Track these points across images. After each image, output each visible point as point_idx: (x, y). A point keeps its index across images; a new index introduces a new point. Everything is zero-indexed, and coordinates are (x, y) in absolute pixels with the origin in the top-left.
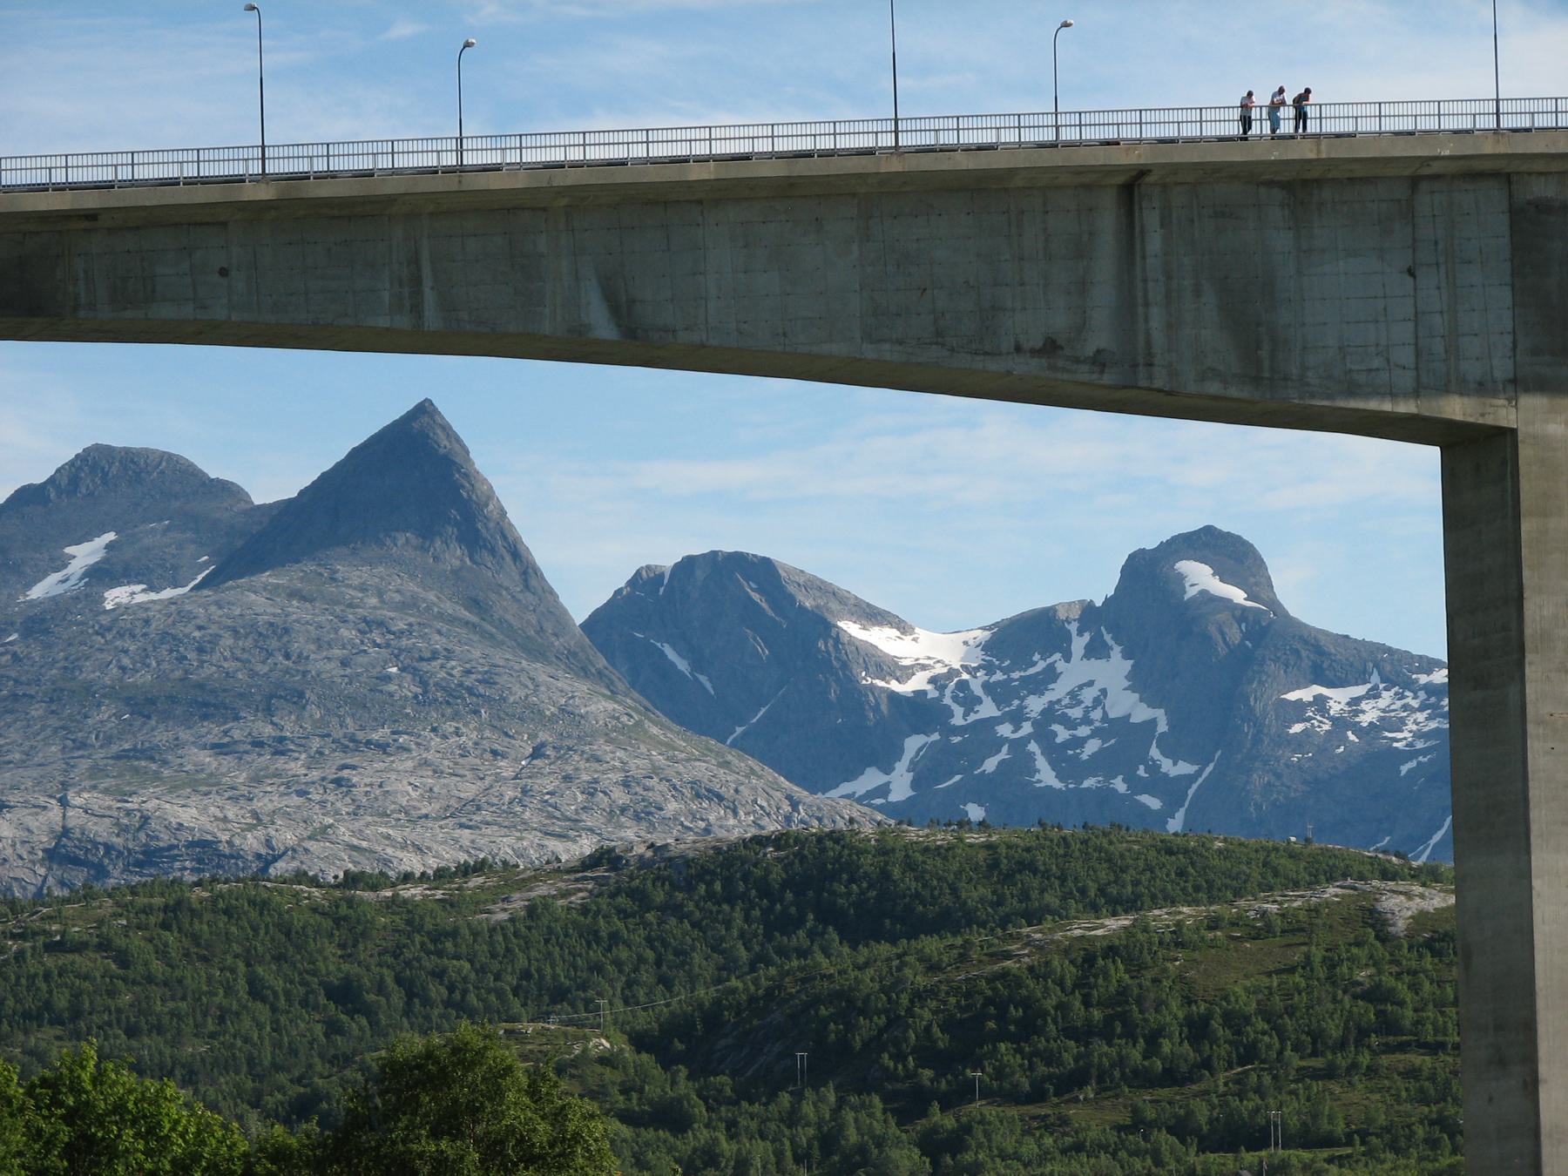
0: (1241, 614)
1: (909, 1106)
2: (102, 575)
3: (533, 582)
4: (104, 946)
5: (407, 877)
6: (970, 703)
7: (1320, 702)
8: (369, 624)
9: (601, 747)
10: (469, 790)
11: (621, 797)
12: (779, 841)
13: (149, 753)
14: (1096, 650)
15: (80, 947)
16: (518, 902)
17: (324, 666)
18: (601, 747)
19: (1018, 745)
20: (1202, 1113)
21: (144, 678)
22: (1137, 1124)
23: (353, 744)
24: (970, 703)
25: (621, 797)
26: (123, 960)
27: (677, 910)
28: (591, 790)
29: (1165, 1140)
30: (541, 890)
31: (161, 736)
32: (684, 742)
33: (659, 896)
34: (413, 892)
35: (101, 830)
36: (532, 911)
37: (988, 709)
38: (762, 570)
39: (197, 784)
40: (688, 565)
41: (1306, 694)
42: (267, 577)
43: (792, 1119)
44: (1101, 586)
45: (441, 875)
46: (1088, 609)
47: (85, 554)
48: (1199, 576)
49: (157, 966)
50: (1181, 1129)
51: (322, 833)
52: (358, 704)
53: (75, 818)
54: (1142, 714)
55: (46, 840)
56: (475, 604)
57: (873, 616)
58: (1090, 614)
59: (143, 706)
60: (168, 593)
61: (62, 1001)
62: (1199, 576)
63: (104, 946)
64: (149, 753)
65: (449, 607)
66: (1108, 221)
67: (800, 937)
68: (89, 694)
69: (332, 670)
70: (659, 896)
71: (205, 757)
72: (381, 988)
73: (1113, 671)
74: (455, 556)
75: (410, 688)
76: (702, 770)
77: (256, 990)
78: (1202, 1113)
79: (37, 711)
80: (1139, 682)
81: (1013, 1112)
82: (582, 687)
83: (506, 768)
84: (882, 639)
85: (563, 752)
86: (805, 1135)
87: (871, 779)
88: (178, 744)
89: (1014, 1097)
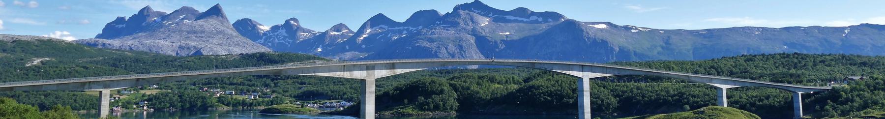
4: (193, 62)
5: (222, 55)
6: (270, 33)
9: (234, 38)
10: (221, 42)
11: (236, 43)
12: (258, 53)
13: (189, 37)
15: (190, 62)
16: (233, 58)
17: (207, 29)
18: (234, 38)
20: (299, 81)
21: (188, 30)
22: (294, 82)
23: (209, 37)
24: (270, 33)
25: (236, 43)
27: (248, 59)
28: (233, 42)
29: (296, 84)
30: (235, 57)
32: (242, 37)
33: (247, 58)
35: (184, 45)
37: (271, 34)
38: (250, 20)
39: (194, 40)
40: (242, 20)
41: (302, 34)
43: (262, 81)
44: (283, 23)
45: (225, 55)
46: (282, 25)
47: (182, 17)
48: (292, 22)
49: (198, 64)
50: (298, 83)
51: (206, 46)
52: (210, 33)
53: (181, 44)
56: (222, 23)
57: (261, 25)
59: (188, 32)
60: (191, 21)
61: (189, 67)
62: (292, 22)
64: (189, 37)
65: (290, 66)
67: (260, 62)
68: (183, 31)
69: (208, 30)
70: (247, 58)
71: (194, 38)
72: (220, 66)
74: (220, 18)
75: (215, 31)
76: (244, 40)
77: (208, 66)
78: (299, 81)
80: (286, 32)
81: (282, 81)
82: (232, 32)
83: (225, 40)
84: (261, 27)
86: (263, 82)
88: (191, 36)
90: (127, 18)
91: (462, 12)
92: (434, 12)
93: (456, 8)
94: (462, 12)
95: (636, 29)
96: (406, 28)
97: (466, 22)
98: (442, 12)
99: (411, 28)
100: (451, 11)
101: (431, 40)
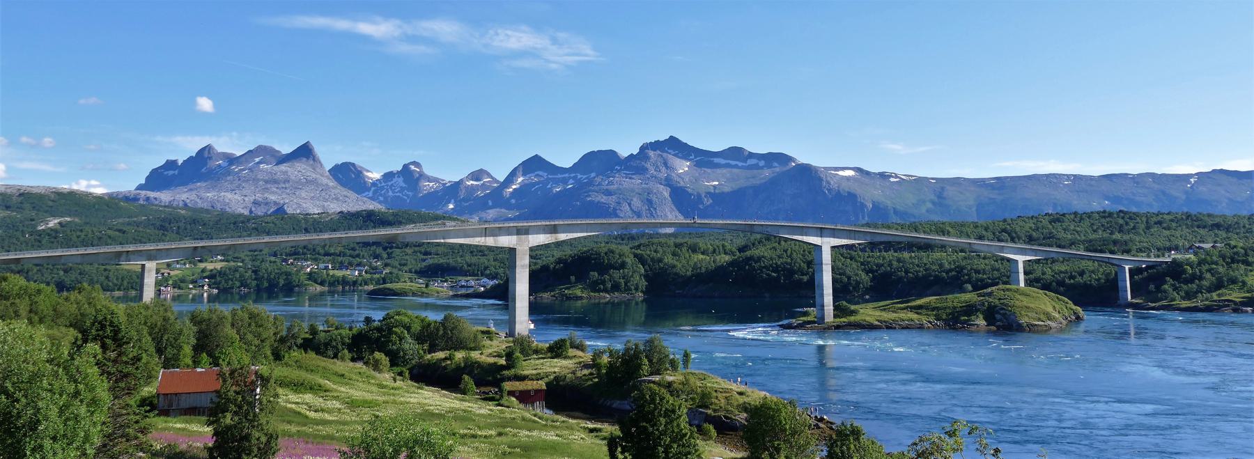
0: (418, 173)
1: (385, 249)
2: (260, 163)
3: (316, 159)
4: (273, 223)
6: (381, 183)
7: (429, 185)
8: (299, 171)
12: (365, 211)
16: (329, 218)
18: (331, 190)
19: (387, 189)
20: (423, 250)
23: (296, 188)
24: (381, 183)
26: (276, 225)
28: (330, 195)
31: (269, 186)
34: (315, 216)
35: (260, 200)
36: (331, 219)
37: (383, 184)
38: (353, 165)
39: (273, 193)
41: (427, 184)
42: (285, 164)
44: (400, 169)
48: (412, 167)
54: (404, 185)
55: (252, 201)
56: (314, 169)
57: (368, 171)
59: (266, 182)
61: (267, 230)
62: (412, 167)
63: (273, 223)
66: (484, 231)
71: (275, 189)
73: (401, 179)
74: (312, 162)
75: (305, 181)
76: (345, 193)
77: (294, 229)
79: (251, 182)
80: (404, 181)
85: (326, 190)
87: (367, 193)
89: (399, 248)
91: (651, 153)
94: (651, 153)
95: (896, 176)
97: (657, 167)
98: (624, 152)
100: (635, 151)
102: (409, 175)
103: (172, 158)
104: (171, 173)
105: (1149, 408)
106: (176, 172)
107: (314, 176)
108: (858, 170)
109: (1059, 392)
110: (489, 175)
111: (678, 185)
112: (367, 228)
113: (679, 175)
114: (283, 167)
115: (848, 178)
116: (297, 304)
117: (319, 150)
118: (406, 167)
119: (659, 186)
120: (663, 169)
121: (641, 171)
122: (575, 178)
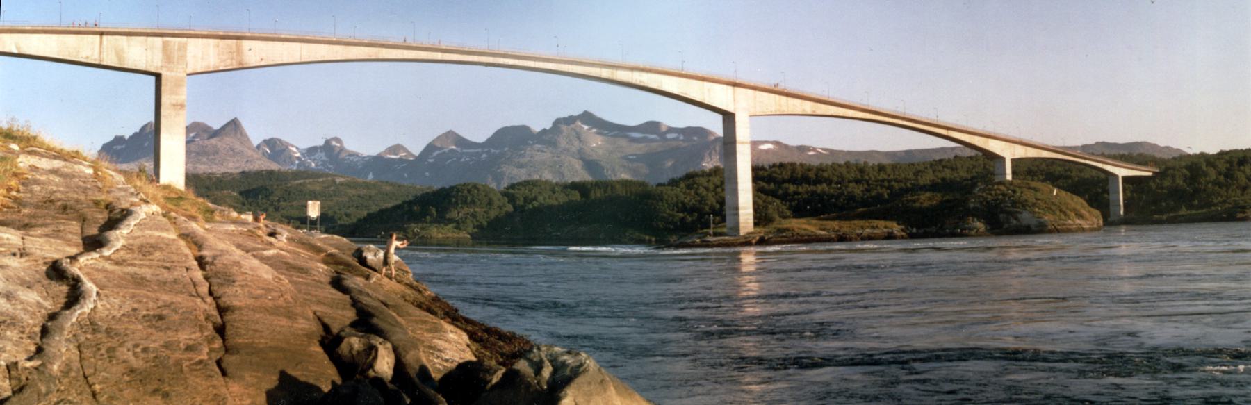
14: (321, 152)
38: (280, 140)
39: (204, 163)
48: (334, 143)
58: (321, 147)
59: (198, 154)
73: (323, 155)
90: (127, 137)
91: (564, 128)
92: (524, 130)
93: (558, 123)
94: (564, 128)
95: (814, 149)
96: (486, 150)
97: (570, 140)
98: (537, 128)
99: (493, 151)
100: (548, 126)
101: (521, 166)
102: (329, 148)
103: (120, 134)
104: (119, 147)
105: (795, 378)
106: (124, 146)
107: (241, 149)
108: (777, 143)
109: (1086, 323)
110: (405, 150)
111: (591, 158)
112: (662, 248)
113: (593, 149)
114: (213, 141)
115: (767, 151)
116: (113, 246)
117: (247, 126)
118: (328, 142)
119: (571, 159)
120: (576, 143)
121: (553, 144)
122: (487, 153)
